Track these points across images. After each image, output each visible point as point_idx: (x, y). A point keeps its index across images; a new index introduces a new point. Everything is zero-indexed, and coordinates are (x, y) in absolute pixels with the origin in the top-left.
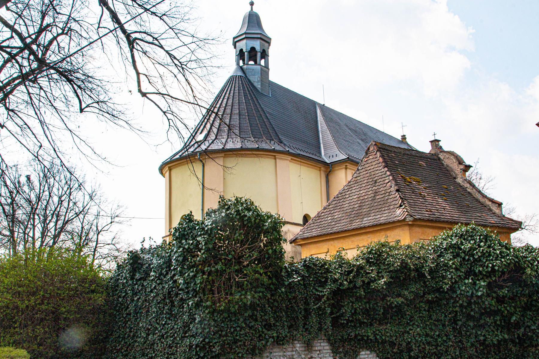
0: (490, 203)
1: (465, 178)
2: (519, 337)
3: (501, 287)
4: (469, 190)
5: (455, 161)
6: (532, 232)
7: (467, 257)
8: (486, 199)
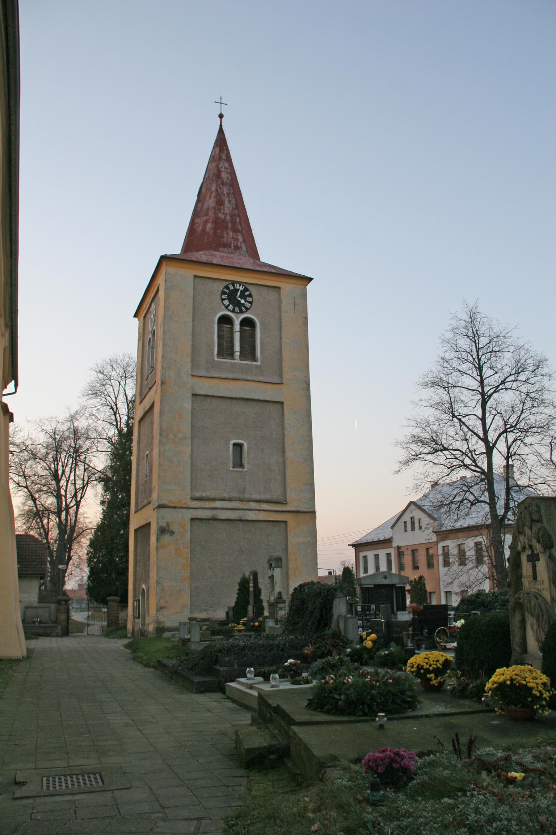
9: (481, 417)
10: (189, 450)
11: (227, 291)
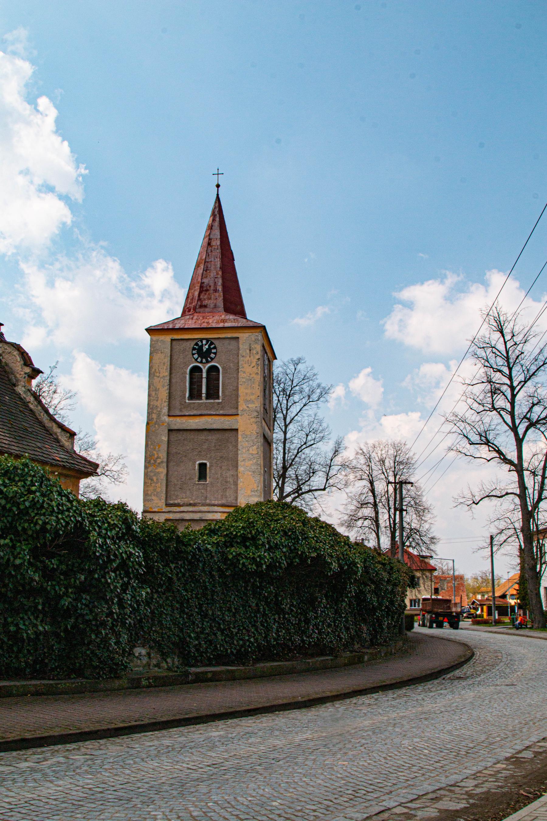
0: (59, 431)
1: (29, 388)
2: (66, 630)
3: (51, 556)
4: (31, 406)
5: (19, 359)
6: (113, 480)
7: (8, 506)
8: (54, 424)
9: (509, 410)
10: (165, 471)
11: (197, 347)
